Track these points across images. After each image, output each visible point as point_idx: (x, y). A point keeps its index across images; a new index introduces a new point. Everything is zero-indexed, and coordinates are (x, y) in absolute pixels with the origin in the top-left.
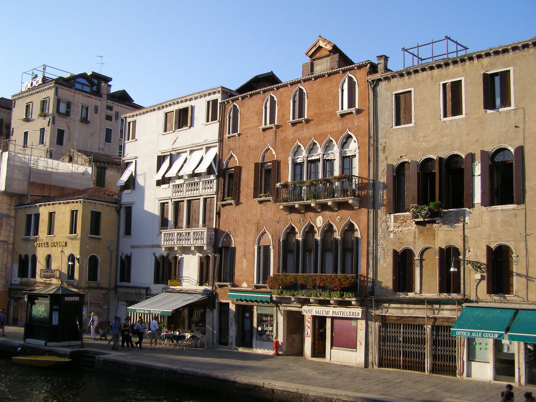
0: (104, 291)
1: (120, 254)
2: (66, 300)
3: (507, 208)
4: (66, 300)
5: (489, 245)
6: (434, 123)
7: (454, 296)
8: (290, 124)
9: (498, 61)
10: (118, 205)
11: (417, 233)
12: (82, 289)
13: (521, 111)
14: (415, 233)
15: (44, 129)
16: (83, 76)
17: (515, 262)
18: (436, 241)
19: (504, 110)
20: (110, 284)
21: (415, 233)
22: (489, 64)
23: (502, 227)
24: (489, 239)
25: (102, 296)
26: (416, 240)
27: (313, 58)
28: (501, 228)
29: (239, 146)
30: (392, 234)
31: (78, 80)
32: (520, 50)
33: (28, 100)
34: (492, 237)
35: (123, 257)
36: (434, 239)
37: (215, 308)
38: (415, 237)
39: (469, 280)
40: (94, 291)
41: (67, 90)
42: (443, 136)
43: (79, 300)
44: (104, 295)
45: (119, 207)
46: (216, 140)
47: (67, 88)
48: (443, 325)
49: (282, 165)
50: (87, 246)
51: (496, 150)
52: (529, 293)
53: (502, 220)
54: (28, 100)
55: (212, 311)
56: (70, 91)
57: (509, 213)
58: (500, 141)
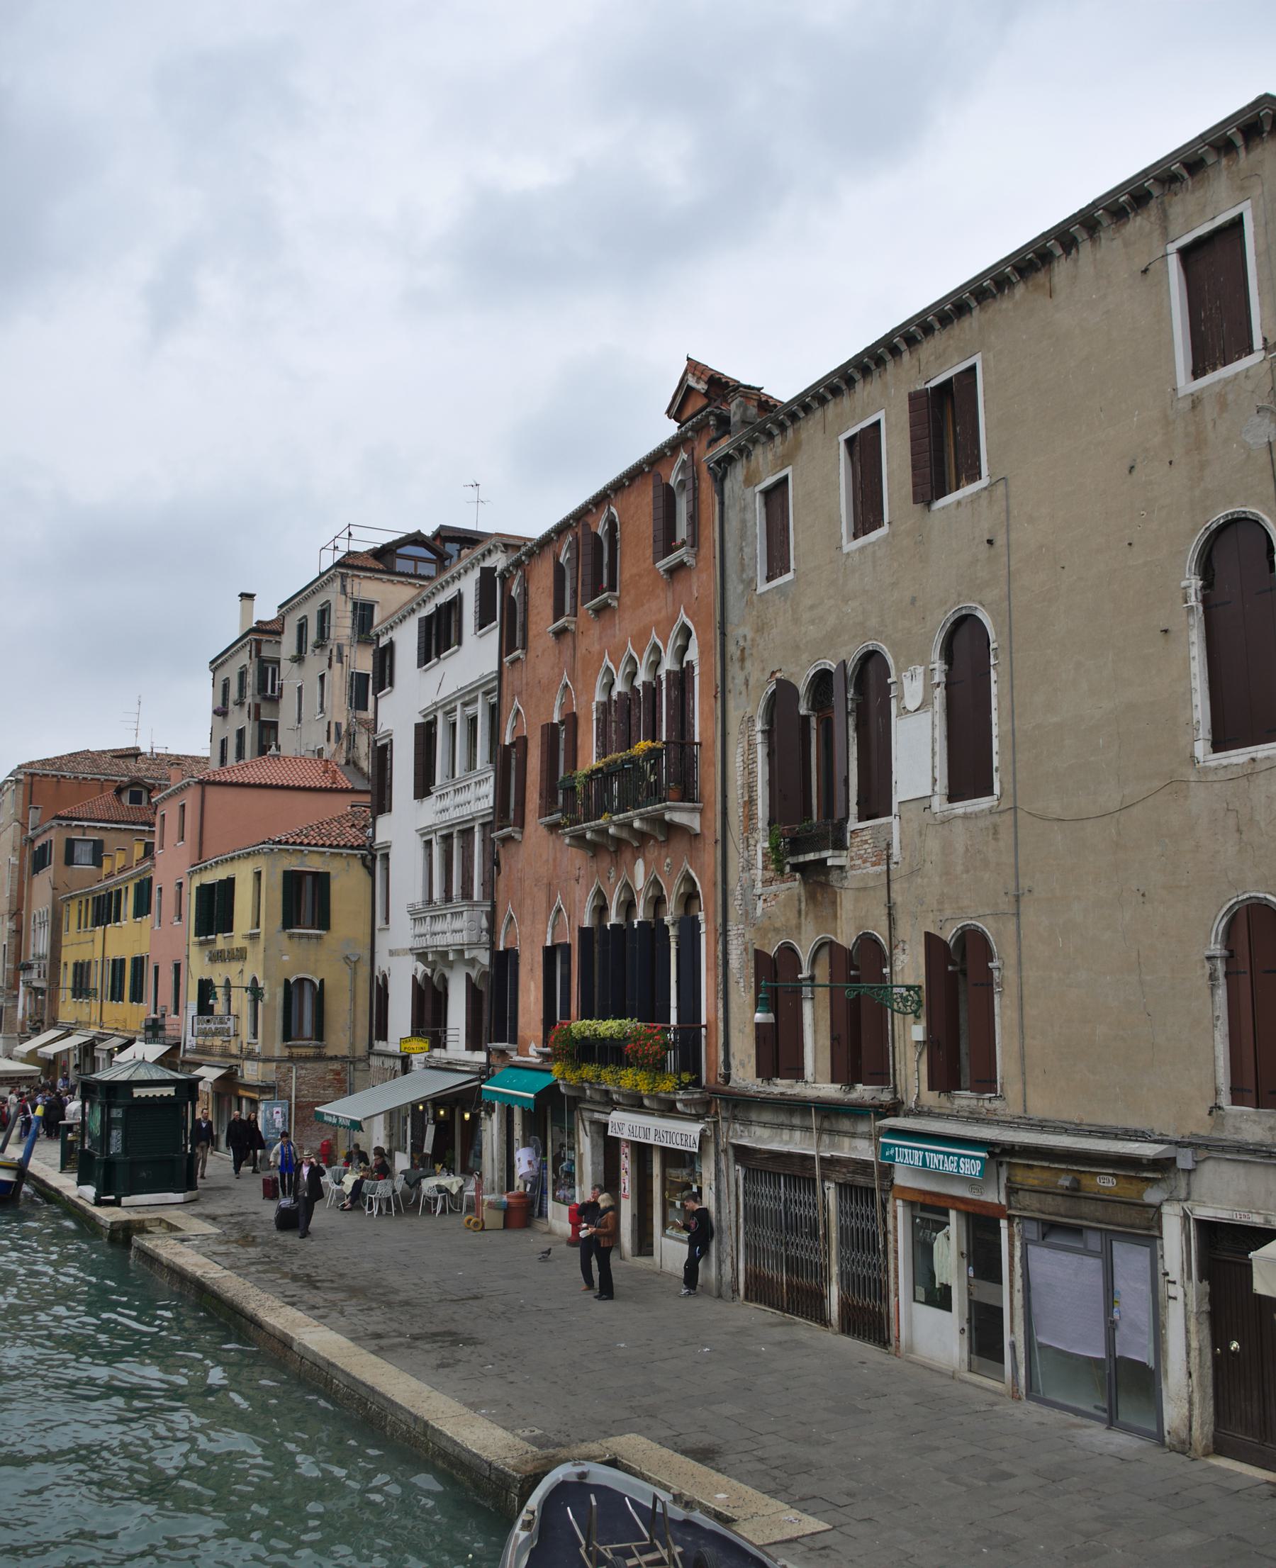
0: (336, 1066)
1: (377, 973)
2: (136, 1095)
3: (976, 808)
4: (136, 1095)
5: (937, 933)
6: (831, 562)
7: (863, 1092)
8: (590, 612)
9: (951, 342)
10: (365, 852)
11: (803, 899)
12: (274, 1061)
13: (1001, 489)
14: (799, 900)
15: (324, 675)
16: (416, 539)
17: (999, 985)
18: (839, 921)
19: (967, 494)
20: (353, 1046)
21: (799, 900)
22: (933, 357)
23: (967, 872)
24: (940, 910)
25: (330, 1077)
26: (803, 917)
27: (684, 417)
28: (965, 876)
29: (527, 684)
30: (760, 904)
31: (400, 551)
32: (994, 297)
33: (299, 614)
34: (946, 906)
35: (419, 977)
36: (835, 917)
37: (494, 1111)
38: (800, 912)
39: (902, 1044)
40: (308, 1065)
41: (370, 578)
42: (846, 600)
43: (173, 1094)
44: (338, 1073)
45: (370, 857)
46: (492, 673)
47: (368, 575)
48: (855, 1183)
49: (582, 722)
50: (285, 958)
51: (953, 623)
52: (1030, 1091)
53: (967, 850)
54: (299, 614)
55: (491, 1116)
56: (388, 580)
57: (982, 823)
58: (959, 595)
